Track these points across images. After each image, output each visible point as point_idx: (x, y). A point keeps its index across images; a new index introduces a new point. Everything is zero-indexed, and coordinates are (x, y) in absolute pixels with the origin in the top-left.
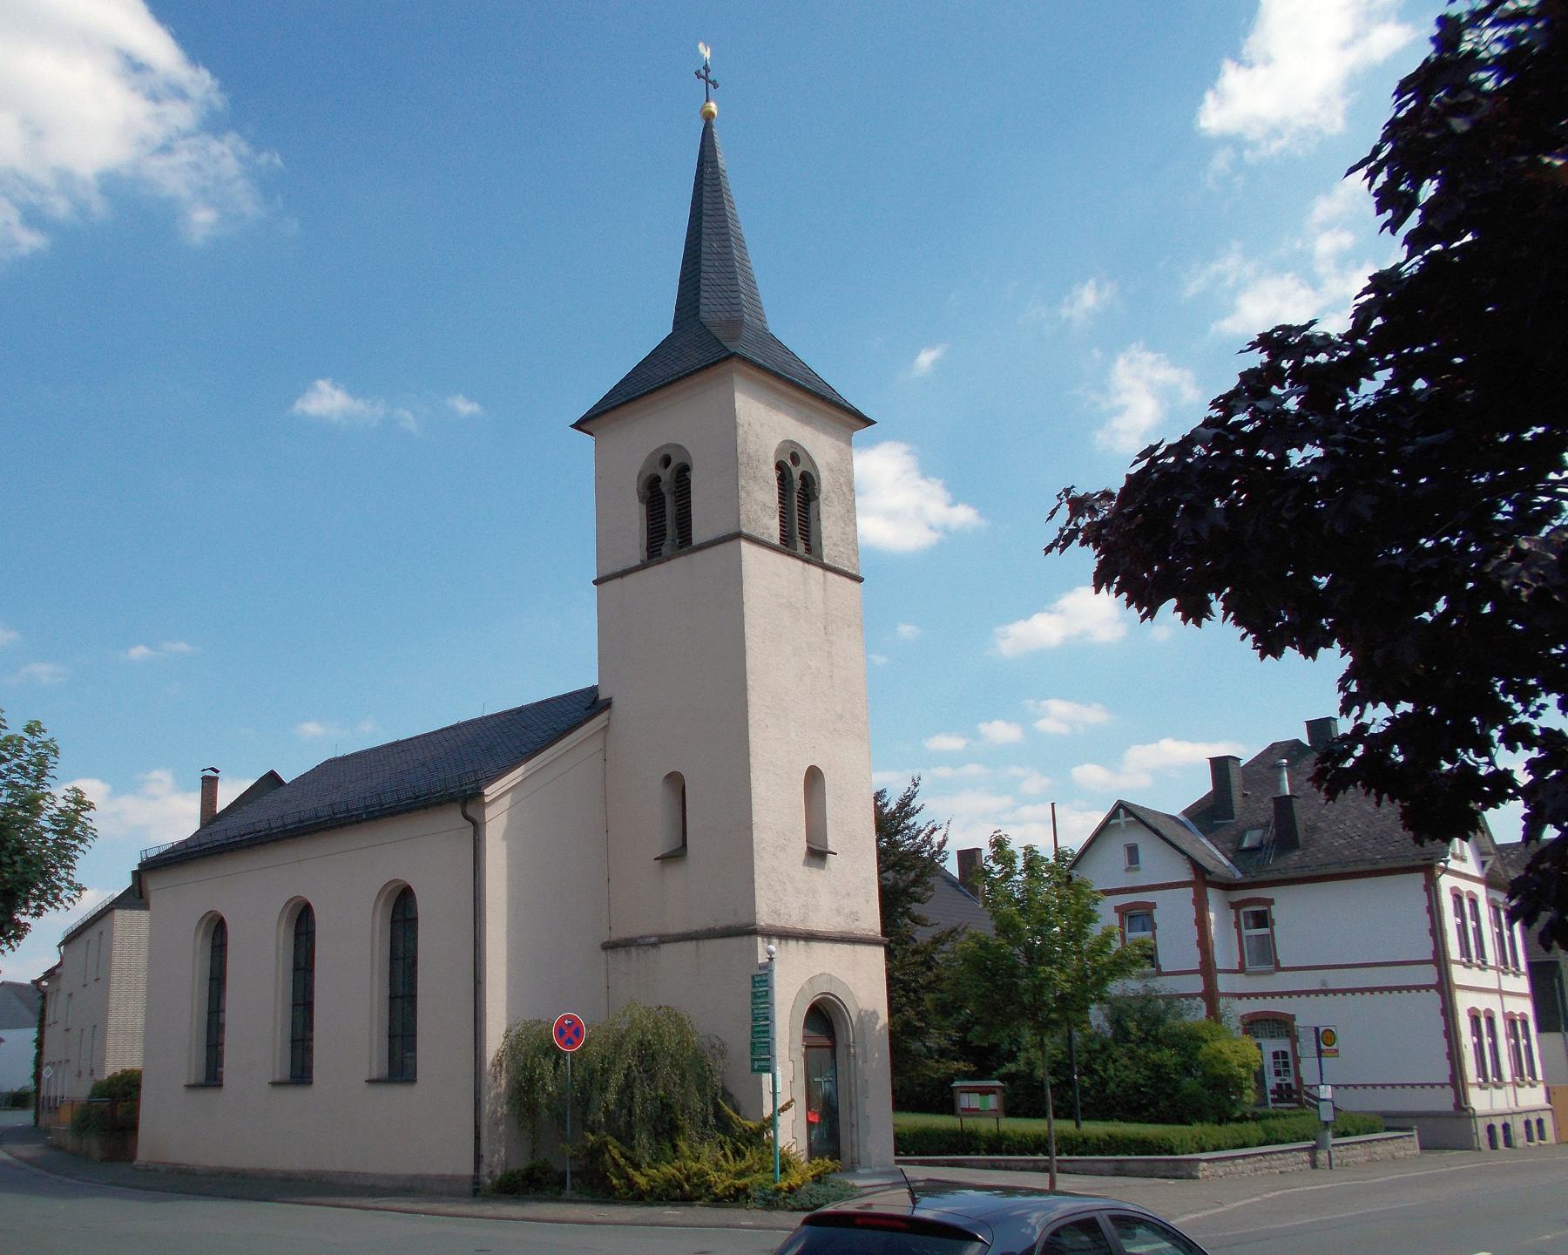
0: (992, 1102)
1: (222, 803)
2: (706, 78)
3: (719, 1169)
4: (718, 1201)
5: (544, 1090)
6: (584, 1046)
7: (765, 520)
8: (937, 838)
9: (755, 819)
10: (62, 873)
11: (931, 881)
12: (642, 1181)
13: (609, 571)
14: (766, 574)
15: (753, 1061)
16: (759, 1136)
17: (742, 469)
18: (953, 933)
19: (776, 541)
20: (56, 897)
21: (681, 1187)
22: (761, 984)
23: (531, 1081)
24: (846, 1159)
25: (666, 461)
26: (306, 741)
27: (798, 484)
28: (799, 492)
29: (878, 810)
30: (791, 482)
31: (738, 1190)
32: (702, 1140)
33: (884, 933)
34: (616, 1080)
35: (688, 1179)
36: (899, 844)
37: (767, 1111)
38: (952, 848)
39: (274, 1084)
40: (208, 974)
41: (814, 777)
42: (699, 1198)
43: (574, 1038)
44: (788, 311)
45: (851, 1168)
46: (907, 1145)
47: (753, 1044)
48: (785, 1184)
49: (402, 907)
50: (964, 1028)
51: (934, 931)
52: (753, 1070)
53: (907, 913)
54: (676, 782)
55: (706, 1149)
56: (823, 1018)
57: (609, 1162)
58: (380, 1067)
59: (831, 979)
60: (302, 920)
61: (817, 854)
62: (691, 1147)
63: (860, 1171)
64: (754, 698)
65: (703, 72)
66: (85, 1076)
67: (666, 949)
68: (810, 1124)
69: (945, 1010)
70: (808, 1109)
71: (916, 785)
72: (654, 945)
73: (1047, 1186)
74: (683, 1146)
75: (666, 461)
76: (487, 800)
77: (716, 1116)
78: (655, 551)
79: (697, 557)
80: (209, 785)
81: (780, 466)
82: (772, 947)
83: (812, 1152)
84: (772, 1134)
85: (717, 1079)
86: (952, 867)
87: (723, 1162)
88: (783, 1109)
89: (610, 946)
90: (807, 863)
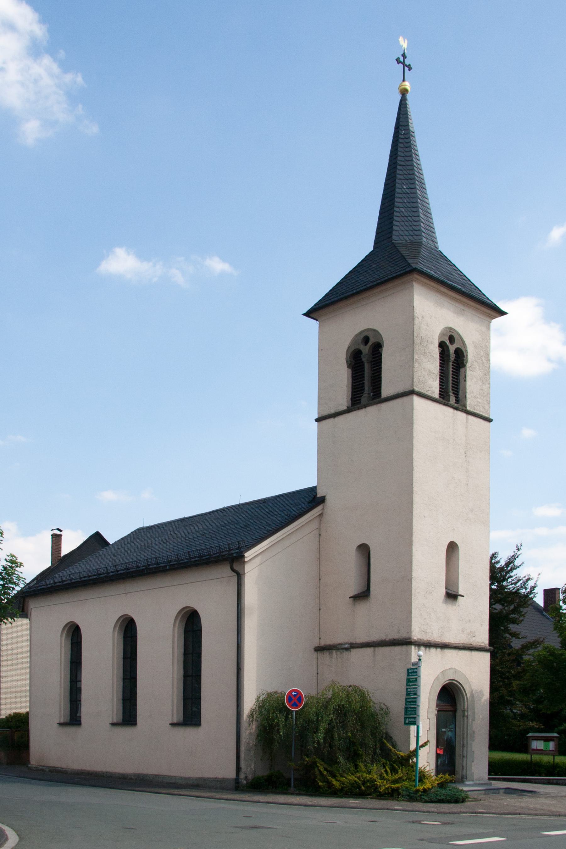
0: (551, 746)
1: (66, 549)
2: (403, 63)
3: (382, 778)
4: (381, 796)
5: (279, 733)
6: (303, 707)
7: (430, 382)
8: (531, 583)
9: (414, 574)
11: (524, 610)
12: (336, 784)
13: (326, 413)
14: (429, 418)
15: (405, 718)
16: (407, 761)
17: (416, 348)
18: (534, 644)
19: (436, 395)
21: (360, 788)
22: (412, 676)
23: (271, 726)
24: (459, 776)
25: (366, 340)
26: (121, 513)
27: (452, 357)
28: (453, 360)
29: (492, 567)
30: (448, 355)
32: (372, 763)
33: (491, 643)
34: (323, 727)
35: (364, 783)
37: (413, 747)
39: (113, 724)
40: (69, 659)
41: (452, 547)
42: (369, 794)
43: (298, 703)
44: (454, 235)
45: (462, 780)
46: (496, 769)
47: (406, 709)
48: (422, 788)
49: (191, 623)
50: (538, 701)
52: (405, 723)
53: (507, 630)
54: (364, 550)
55: (375, 767)
56: (450, 695)
57: (317, 773)
58: (178, 717)
59: (456, 671)
60: (128, 629)
61: (452, 596)
62: (366, 766)
63: (467, 783)
64: (417, 498)
65: (401, 59)
67: (354, 652)
68: (438, 756)
69: (525, 691)
70: (437, 746)
71: (519, 550)
72: (347, 649)
74: (361, 765)
76: (246, 560)
77: (381, 749)
79: (384, 406)
81: (442, 345)
82: (421, 653)
83: (438, 772)
84: (415, 760)
85: (383, 728)
86: (539, 600)
87: (385, 775)
88: (423, 746)
89: (319, 649)
90: (445, 602)
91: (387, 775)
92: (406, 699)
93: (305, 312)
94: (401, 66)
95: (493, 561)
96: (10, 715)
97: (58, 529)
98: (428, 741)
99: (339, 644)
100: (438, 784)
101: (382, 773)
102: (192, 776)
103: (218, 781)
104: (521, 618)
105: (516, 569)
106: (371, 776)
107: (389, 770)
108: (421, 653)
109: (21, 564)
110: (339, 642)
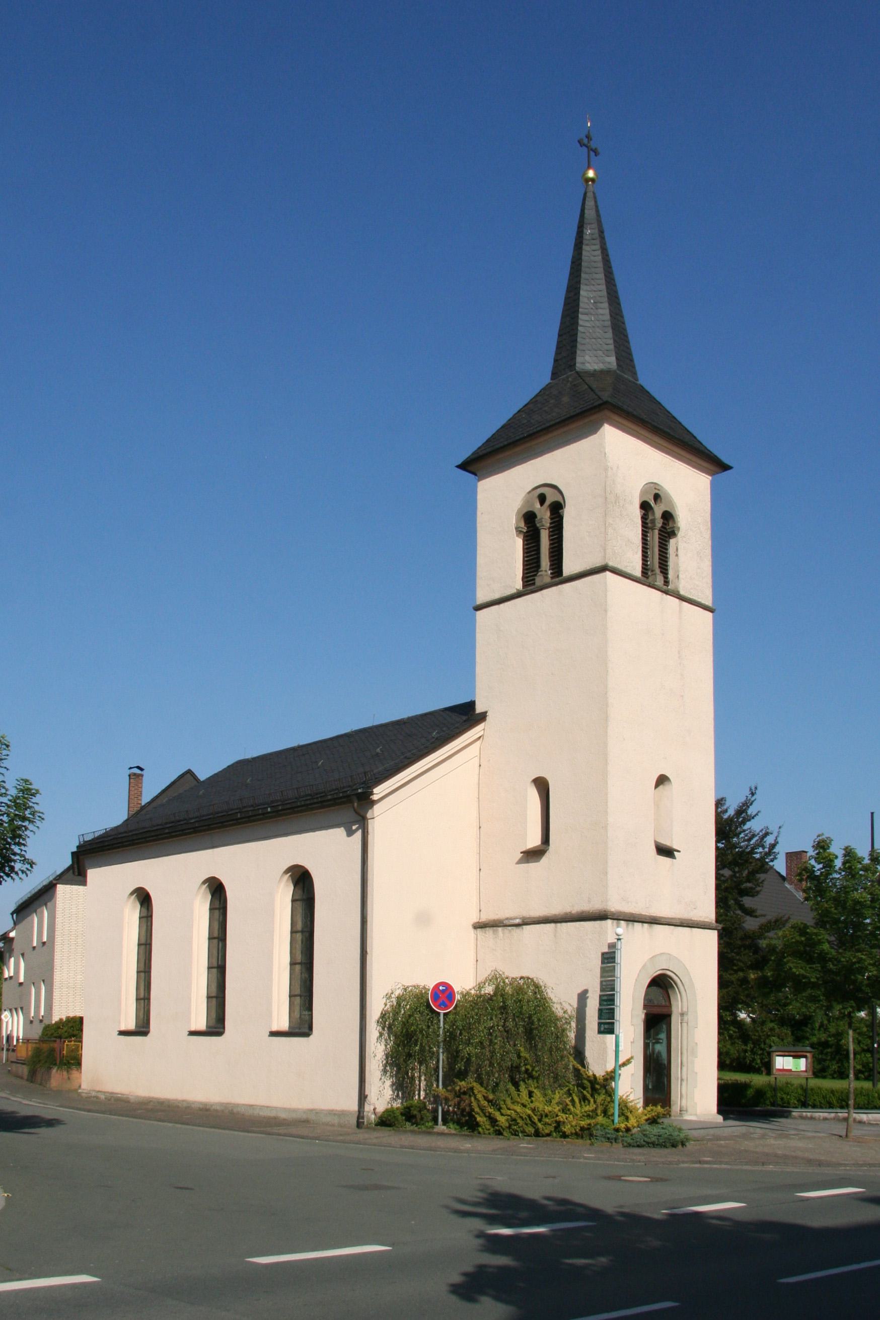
8: (769, 840)
10: (16, 849)
11: (761, 876)
16: (601, 1087)
18: (778, 923)
19: (638, 573)
20: (12, 869)
27: (659, 523)
30: (653, 521)
31: (582, 1129)
33: (717, 921)
36: (735, 846)
38: (782, 850)
43: (448, 1003)
48: (623, 1126)
51: (763, 920)
65: (585, 141)
66: (36, 1023)
71: (753, 794)
72: (517, 925)
73: (843, 1133)
75: (542, 499)
78: (531, 581)
80: (136, 777)
82: (620, 931)
83: (647, 1102)
86: (780, 865)
87: (571, 1107)
88: (624, 1064)
91: (574, 1105)
92: (600, 996)
93: (460, 463)
94: (585, 149)
95: (719, 810)
96: (61, 1020)
97: (138, 768)
98: (632, 1058)
99: (507, 919)
100: (647, 1120)
101: (567, 1105)
102: (300, 1107)
103: (335, 1114)
104: (758, 889)
105: (749, 820)
106: (550, 1109)
107: (576, 1099)
108: (620, 931)
109: (37, 792)
110: (508, 916)
